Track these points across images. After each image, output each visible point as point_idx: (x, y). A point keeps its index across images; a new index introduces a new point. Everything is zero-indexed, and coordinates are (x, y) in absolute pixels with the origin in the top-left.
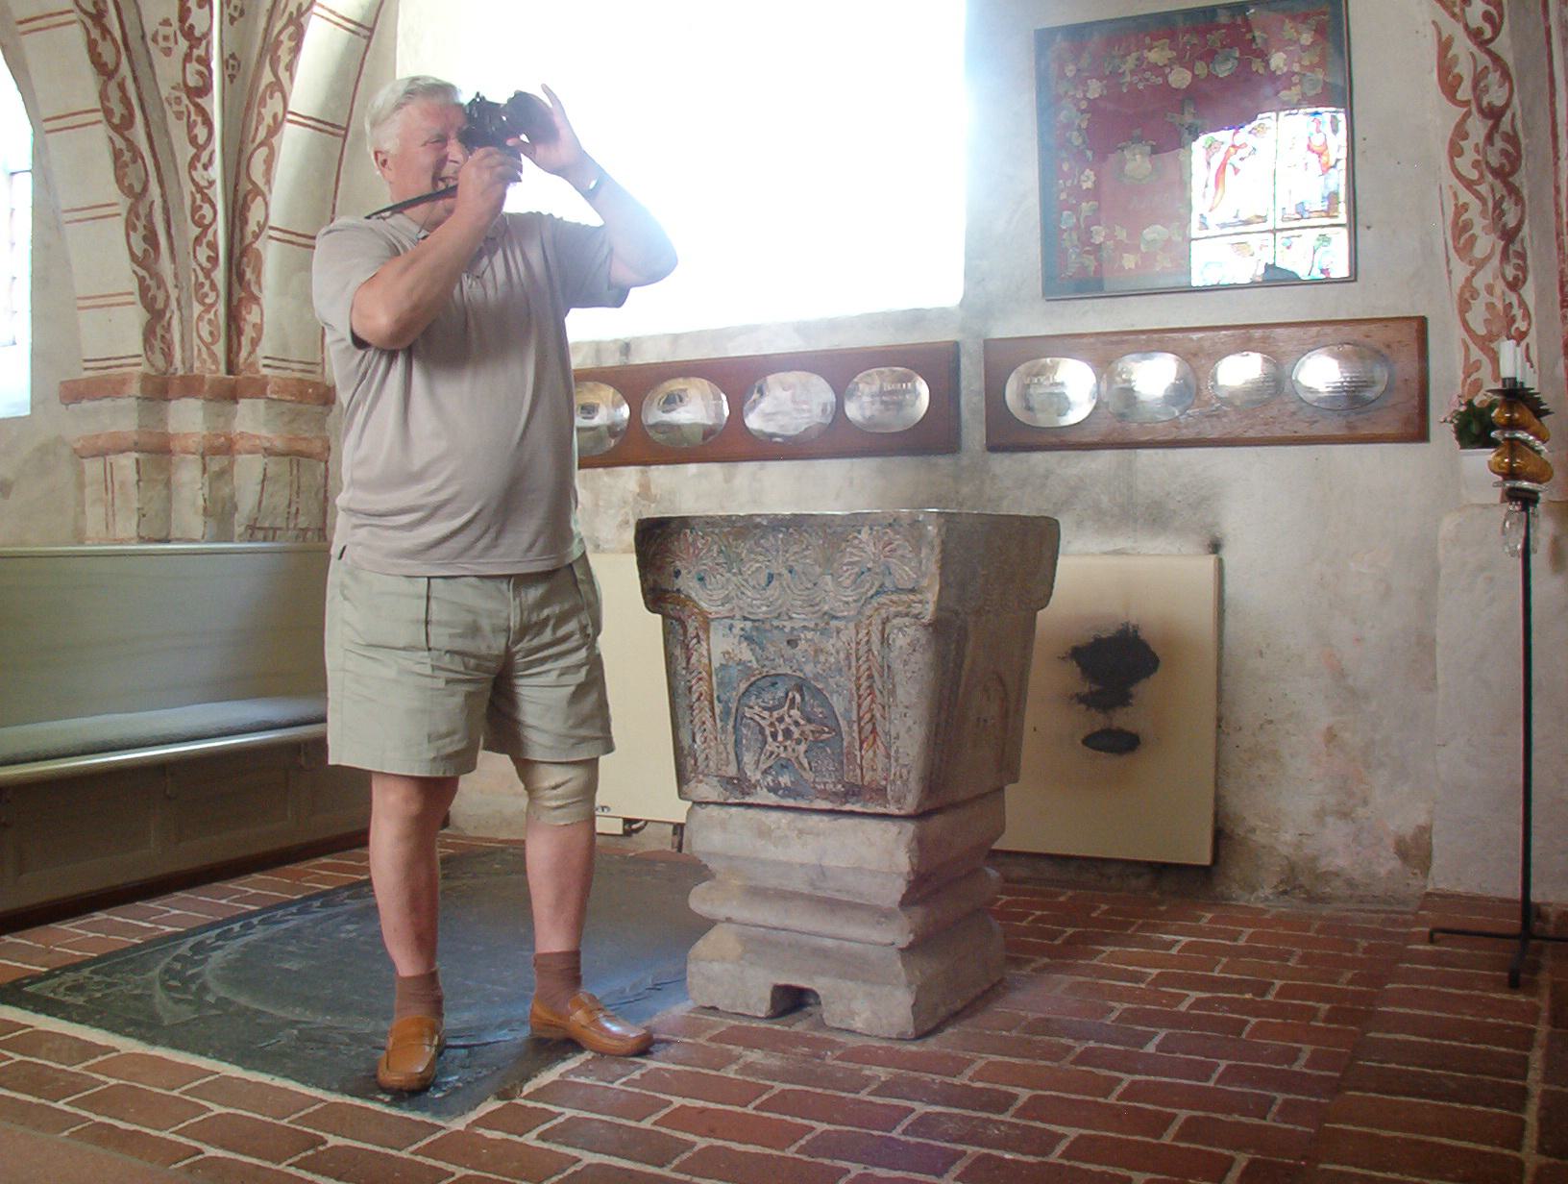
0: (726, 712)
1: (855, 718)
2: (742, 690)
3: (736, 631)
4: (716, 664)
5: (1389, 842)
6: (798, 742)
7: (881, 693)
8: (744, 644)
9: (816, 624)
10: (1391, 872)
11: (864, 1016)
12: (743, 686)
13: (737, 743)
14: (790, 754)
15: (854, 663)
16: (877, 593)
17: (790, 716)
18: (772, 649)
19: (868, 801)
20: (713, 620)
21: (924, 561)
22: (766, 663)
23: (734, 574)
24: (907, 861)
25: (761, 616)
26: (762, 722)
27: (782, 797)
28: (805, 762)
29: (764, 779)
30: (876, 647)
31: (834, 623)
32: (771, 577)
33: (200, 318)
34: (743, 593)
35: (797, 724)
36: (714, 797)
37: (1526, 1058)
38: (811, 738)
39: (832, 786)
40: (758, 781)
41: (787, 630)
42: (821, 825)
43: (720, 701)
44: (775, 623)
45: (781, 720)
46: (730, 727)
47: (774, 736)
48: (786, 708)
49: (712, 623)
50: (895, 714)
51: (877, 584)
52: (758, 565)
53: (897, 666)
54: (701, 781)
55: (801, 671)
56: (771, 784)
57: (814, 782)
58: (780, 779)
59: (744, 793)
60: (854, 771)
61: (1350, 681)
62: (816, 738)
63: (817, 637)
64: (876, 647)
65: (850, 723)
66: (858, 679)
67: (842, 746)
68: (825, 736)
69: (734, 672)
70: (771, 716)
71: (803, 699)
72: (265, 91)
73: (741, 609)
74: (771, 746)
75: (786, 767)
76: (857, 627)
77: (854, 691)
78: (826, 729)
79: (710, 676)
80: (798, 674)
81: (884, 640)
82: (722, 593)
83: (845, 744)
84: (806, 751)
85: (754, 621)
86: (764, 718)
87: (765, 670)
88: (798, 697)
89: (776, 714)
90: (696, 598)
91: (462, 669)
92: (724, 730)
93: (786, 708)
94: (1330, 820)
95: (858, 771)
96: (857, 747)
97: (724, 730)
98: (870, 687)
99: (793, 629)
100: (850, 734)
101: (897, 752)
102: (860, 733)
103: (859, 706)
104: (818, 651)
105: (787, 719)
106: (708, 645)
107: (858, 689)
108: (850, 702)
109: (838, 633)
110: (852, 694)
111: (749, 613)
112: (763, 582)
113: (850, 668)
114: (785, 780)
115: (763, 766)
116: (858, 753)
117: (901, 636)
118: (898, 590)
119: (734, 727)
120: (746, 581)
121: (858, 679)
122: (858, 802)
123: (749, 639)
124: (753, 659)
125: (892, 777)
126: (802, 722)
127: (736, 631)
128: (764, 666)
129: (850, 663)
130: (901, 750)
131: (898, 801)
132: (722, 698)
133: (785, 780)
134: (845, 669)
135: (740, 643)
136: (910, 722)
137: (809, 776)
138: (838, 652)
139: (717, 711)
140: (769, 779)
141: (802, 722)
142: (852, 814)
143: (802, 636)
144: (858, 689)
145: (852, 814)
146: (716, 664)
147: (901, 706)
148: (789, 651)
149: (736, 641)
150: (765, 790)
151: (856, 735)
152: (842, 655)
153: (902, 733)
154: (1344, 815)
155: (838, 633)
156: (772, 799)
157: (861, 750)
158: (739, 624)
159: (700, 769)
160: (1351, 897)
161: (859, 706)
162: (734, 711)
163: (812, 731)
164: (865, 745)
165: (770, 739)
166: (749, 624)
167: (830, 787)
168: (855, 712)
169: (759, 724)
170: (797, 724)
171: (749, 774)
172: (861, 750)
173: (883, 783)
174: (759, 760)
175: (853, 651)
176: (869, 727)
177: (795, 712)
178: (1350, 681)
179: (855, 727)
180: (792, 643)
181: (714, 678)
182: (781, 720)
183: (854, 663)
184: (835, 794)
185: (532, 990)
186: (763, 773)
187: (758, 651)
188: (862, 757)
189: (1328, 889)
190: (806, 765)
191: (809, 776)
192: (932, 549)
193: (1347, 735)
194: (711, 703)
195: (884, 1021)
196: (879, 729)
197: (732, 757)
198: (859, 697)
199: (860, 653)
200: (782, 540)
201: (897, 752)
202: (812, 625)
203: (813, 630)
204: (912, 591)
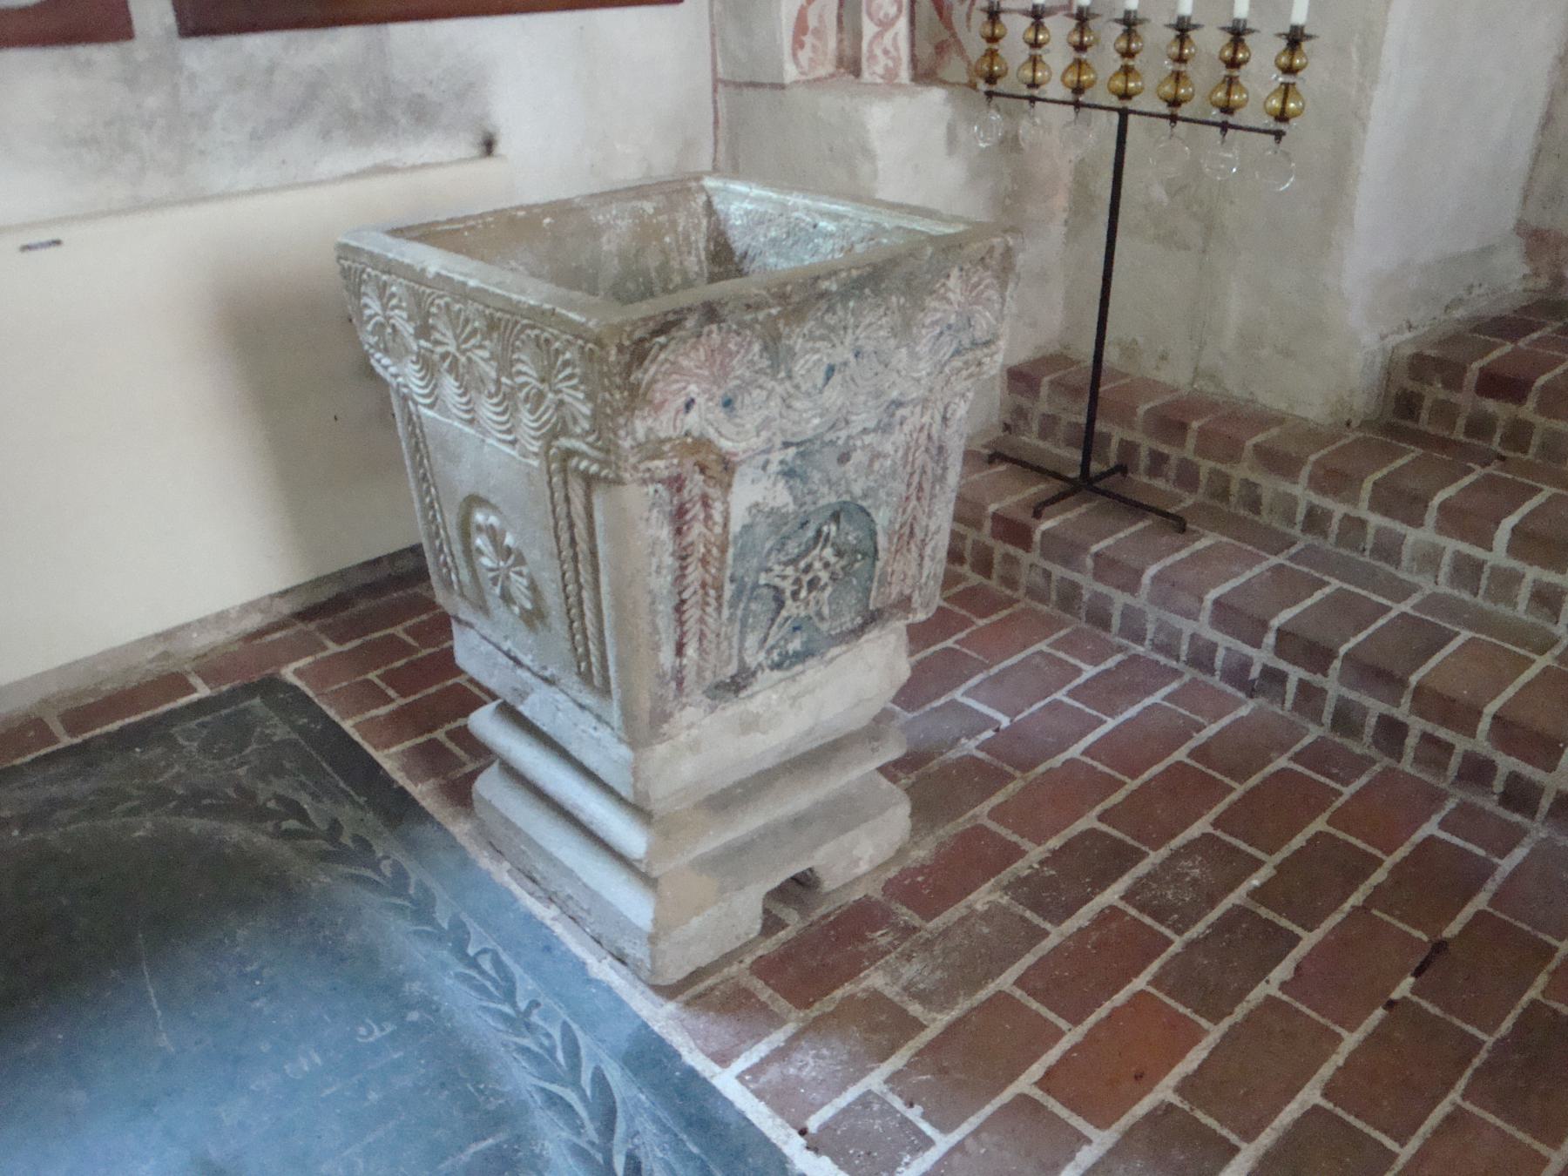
4: (735, 528)
25: (809, 434)
32: (831, 370)
33: (566, 364)
37: (1493, 568)
44: (827, 438)
45: (808, 568)
52: (816, 357)
69: (761, 530)
72: (871, 44)
82: (758, 417)
83: (879, 564)
85: (798, 444)
89: (802, 564)
91: (489, 786)
104: (876, 456)
106: (725, 502)
111: (794, 435)
112: (820, 377)
125: (923, 580)
127: (774, 467)
135: (774, 484)
146: (735, 528)
149: (769, 484)
150: (767, 671)
152: (900, 453)
166: (792, 451)
167: (849, 625)
180: (844, 458)
182: (808, 568)
185: (887, 962)
200: (853, 311)
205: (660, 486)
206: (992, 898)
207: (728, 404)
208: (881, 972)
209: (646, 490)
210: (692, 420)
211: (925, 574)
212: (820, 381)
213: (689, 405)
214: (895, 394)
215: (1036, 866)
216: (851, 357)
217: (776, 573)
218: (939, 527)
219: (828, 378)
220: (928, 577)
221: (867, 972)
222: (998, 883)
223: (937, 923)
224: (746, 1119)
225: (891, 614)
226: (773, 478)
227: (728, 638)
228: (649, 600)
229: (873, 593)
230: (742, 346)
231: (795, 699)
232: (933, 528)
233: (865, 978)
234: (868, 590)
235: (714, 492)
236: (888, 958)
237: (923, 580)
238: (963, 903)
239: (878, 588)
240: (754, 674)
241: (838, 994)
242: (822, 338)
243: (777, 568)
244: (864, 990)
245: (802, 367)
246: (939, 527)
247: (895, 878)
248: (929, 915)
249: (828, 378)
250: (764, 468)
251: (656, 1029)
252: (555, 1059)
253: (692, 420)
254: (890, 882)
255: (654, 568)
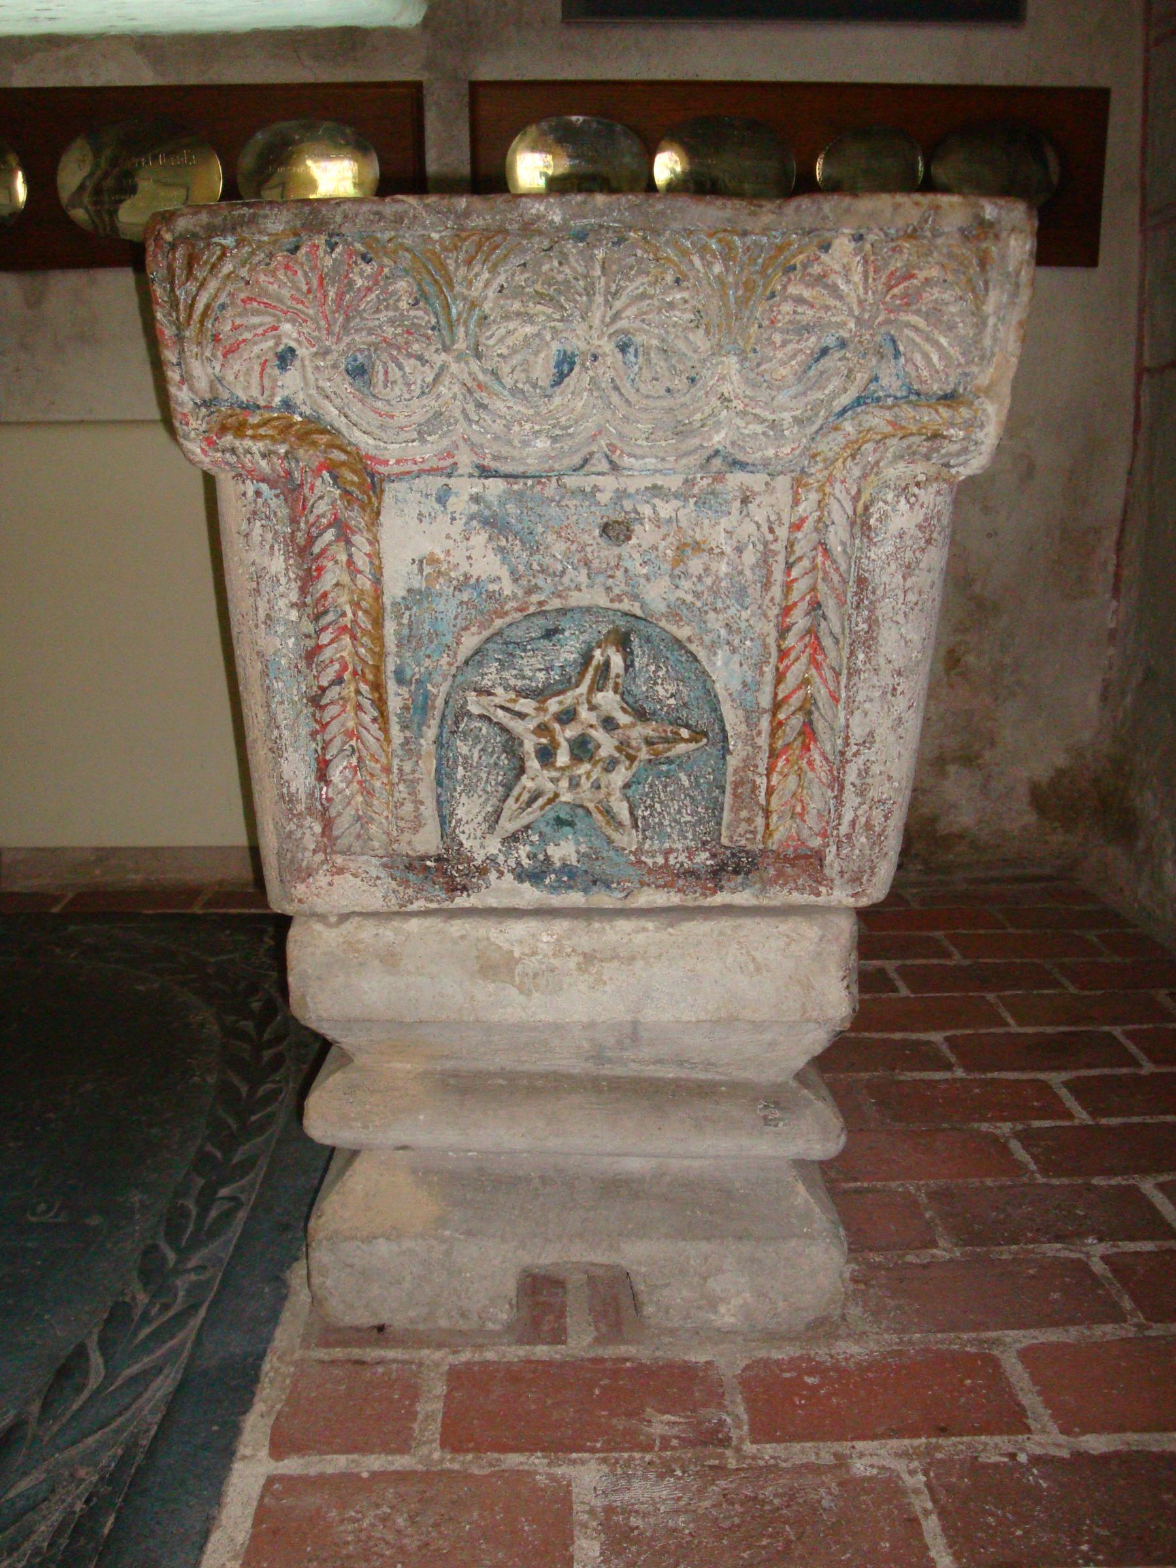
0: (420, 707)
1: (765, 701)
2: (464, 652)
3: (460, 503)
5: (1022, 790)
6: (611, 765)
7: (837, 642)
8: (480, 539)
9: (689, 483)
10: (1024, 828)
11: (736, 1302)
12: (470, 642)
13: (442, 777)
14: (586, 795)
15: (778, 576)
16: (859, 401)
17: (592, 708)
18: (559, 548)
19: (773, 881)
20: (390, 478)
21: (991, 321)
22: (540, 581)
23: (459, 358)
24: (844, 993)
25: (532, 465)
26: (516, 726)
27: (553, 889)
28: (622, 810)
29: (507, 855)
30: (837, 536)
31: (736, 479)
32: (565, 366)
34: (480, 406)
35: (609, 724)
36: (374, 900)
38: (644, 754)
39: (682, 858)
40: (492, 859)
41: (603, 498)
42: (640, 938)
43: (401, 681)
44: (572, 481)
45: (568, 716)
46: (427, 742)
47: (546, 755)
48: (583, 688)
49: (387, 486)
50: (867, 690)
51: (861, 377)
53: (887, 577)
54: (341, 871)
55: (635, 597)
56: (526, 862)
57: (639, 851)
58: (551, 850)
59: (453, 888)
60: (749, 821)
61: (977, 588)
62: (657, 754)
63: (687, 512)
64: (837, 536)
65: (750, 716)
66: (787, 611)
67: (721, 770)
68: (681, 748)
69: (448, 607)
70: (541, 709)
71: (629, 666)
73: (473, 446)
74: (536, 777)
75: (571, 824)
76: (798, 483)
77: (771, 641)
78: (685, 733)
79: (378, 623)
80: (626, 605)
81: (861, 524)
82: (420, 410)
83: (733, 762)
84: (627, 786)
86: (521, 716)
87: (535, 598)
88: (617, 661)
89: (553, 705)
90: (341, 423)
92: (410, 750)
93: (583, 688)
94: (952, 769)
95: (760, 821)
96: (762, 769)
97: (410, 750)
98: (812, 631)
99: (621, 494)
100: (750, 741)
101: (865, 773)
102: (773, 735)
103: (780, 678)
105: (584, 713)
106: (374, 541)
107: (783, 631)
108: (759, 667)
109: (745, 501)
110: (765, 646)
111: (496, 458)
112: (543, 370)
113: (767, 585)
114: (564, 850)
115: (508, 826)
116: (762, 782)
117: (903, 505)
118: (915, 396)
119: (439, 742)
120: (494, 373)
121: (787, 611)
122: (744, 886)
123: (494, 524)
124: (504, 573)
125: (844, 829)
126: (623, 719)
127: (460, 503)
128: (535, 589)
129: (770, 573)
130: (876, 769)
131: (856, 879)
132: (408, 673)
133: (564, 850)
134: (754, 591)
136: (901, 703)
137: (628, 840)
138: (739, 550)
139: (394, 704)
140: (523, 851)
141: (623, 719)
142: (727, 910)
143: (646, 510)
144: (783, 631)
145: (727, 910)
147: (886, 670)
148: (603, 552)
150: (509, 877)
151: (763, 741)
152: (750, 557)
153: (881, 732)
154: (969, 760)
155: (745, 501)
156: (530, 895)
157: (768, 776)
158: (465, 487)
159: (343, 843)
160: (978, 862)
161: (780, 678)
162: (440, 702)
163: (649, 742)
164: (781, 763)
165: (533, 764)
166: (495, 487)
168: (768, 689)
169: (504, 729)
170: (609, 724)
171: (467, 844)
172: (768, 776)
173: (816, 842)
174: (498, 813)
175: (779, 547)
176: (797, 722)
177: (607, 699)
178: (977, 588)
179: (765, 723)
181: (390, 627)
183: (778, 576)
184: (691, 873)
186: (504, 841)
187: (520, 555)
188: (770, 791)
189: (951, 857)
190: (624, 814)
191: (628, 840)
192: (1015, 294)
193: (971, 659)
194: (378, 686)
195: (781, 1304)
196: (820, 726)
197: (429, 810)
198: (783, 654)
199: (799, 550)
201: (865, 773)
202: (674, 483)
203: (676, 496)
204: (950, 398)
205: (264, 487)
206: (900, 1466)
207: (359, 372)
208: (605, 1469)
209: (242, 488)
210: (290, 383)
211: (848, 816)
212: (545, 380)
213: (285, 358)
214: (718, 439)
215: (1022, 1458)
216: (608, 347)
217: (497, 701)
218: (871, 734)
219: (560, 378)
220: (853, 823)
221: (586, 1455)
222: (930, 1450)
223: (769, 1450)
224: (206, 1535)
225: (780, 874)
226: (460, 524)
227: (412, 784)
228: (259, 666)
229: (727, 816)
230: (376, 283)
231: (589, 958)
232: (858, 732)
233: (574, 1462)
234: (716, 808)
235: (356, 518)
236: (637, 1455)
237: (844, 829)
238: (837, 1447)
239: (736, 810)
240: (482, 871)
241: (513, 1460)
242: (540, 297)
243: (501, 696)
244: (552, 1477)
245: (501, 340)
246: (871, 734)
247: (778, 1362)
248: (763, 1432)
249: (560, 378)
250: (442, 500)
251: (266, 1366)
252: (138, 1328)
253: (290, 383)
254: (766, 1363)
255: (262, 615)
